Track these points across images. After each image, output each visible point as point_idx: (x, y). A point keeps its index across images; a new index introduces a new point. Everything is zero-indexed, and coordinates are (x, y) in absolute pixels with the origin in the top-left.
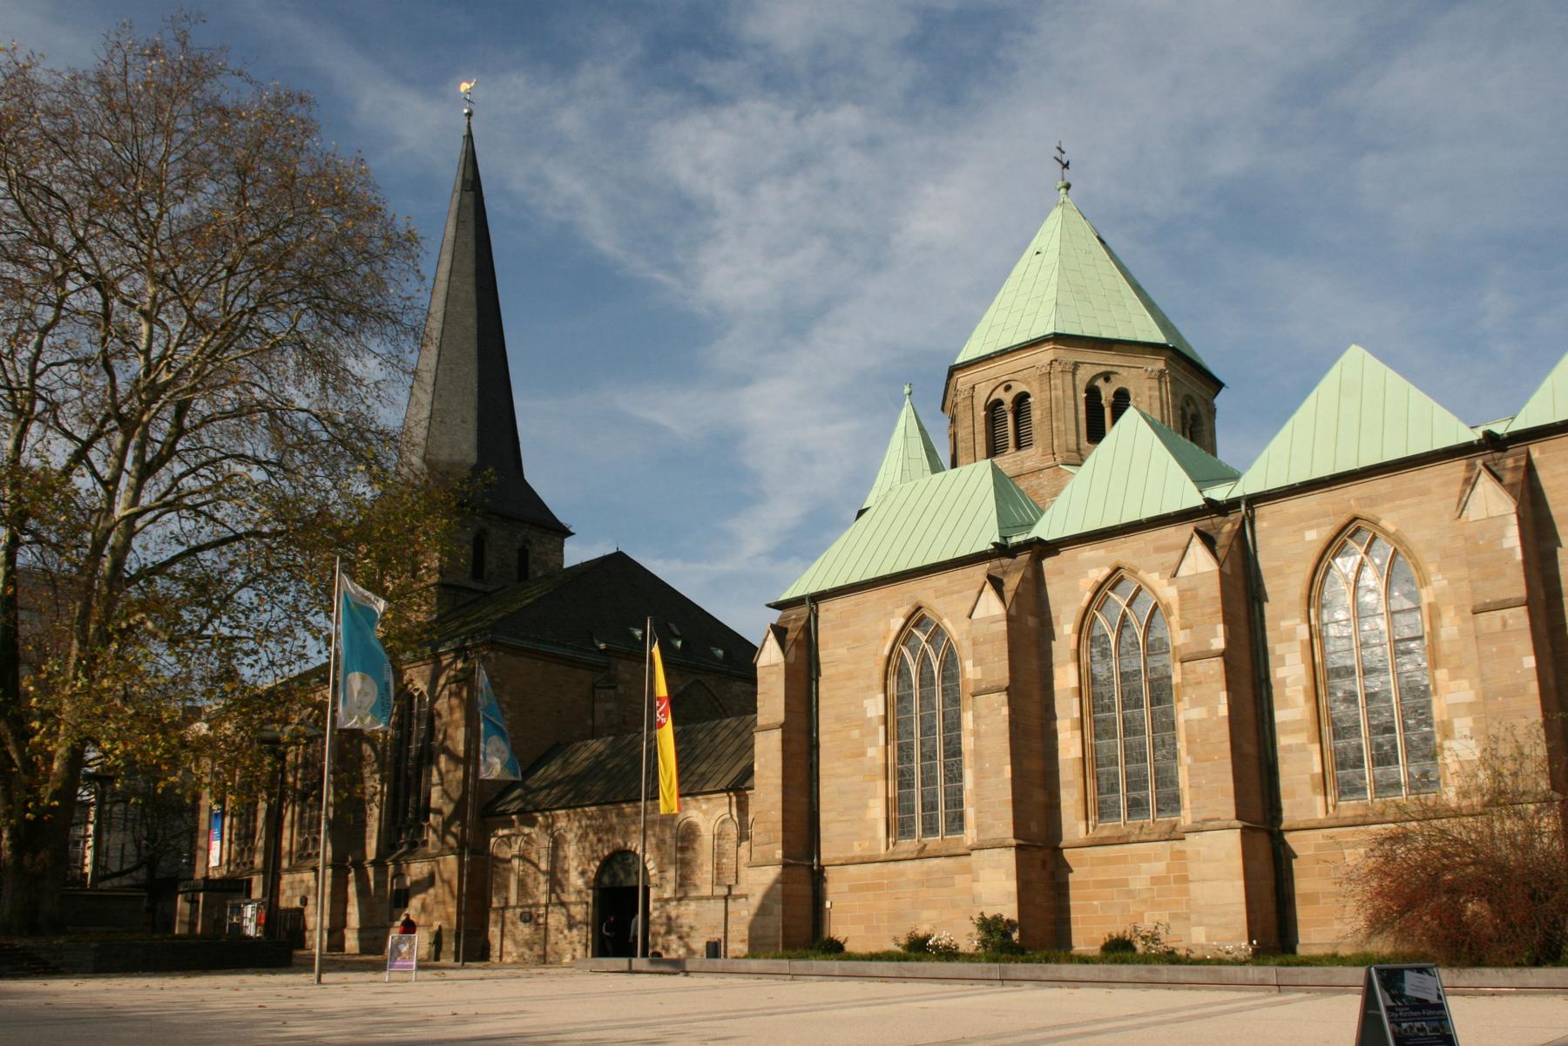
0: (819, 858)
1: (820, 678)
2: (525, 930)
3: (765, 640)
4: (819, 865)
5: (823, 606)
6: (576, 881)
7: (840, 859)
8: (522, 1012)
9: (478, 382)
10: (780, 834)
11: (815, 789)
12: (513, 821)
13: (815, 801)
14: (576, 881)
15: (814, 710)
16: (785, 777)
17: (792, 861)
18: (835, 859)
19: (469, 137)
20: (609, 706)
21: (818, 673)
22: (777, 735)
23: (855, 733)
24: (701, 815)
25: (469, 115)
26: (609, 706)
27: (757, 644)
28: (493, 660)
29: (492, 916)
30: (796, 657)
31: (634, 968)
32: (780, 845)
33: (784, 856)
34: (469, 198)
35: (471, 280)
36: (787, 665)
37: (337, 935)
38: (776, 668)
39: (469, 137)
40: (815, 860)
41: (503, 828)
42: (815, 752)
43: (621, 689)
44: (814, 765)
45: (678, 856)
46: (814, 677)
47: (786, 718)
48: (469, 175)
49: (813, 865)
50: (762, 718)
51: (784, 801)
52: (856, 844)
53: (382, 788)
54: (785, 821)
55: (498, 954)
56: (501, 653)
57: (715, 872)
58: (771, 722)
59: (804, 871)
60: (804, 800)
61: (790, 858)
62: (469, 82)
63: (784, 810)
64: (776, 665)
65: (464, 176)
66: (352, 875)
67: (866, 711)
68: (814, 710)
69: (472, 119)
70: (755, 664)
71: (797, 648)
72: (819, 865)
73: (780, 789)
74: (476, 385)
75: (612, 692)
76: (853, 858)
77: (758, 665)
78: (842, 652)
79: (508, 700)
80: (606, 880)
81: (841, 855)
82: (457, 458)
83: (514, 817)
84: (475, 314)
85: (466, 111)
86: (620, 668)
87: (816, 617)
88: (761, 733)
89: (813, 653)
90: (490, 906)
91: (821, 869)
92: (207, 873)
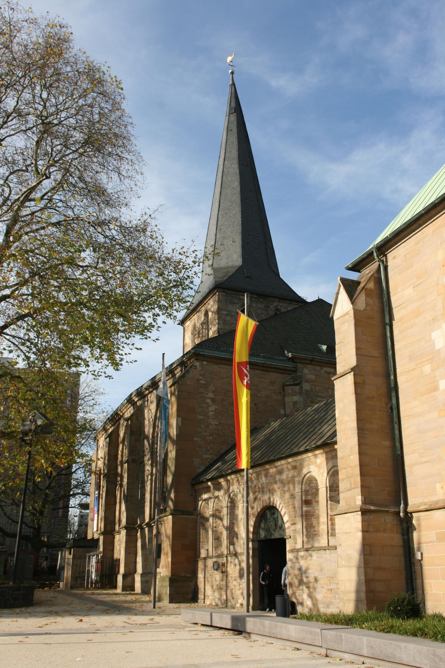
0: (406, 504)
1: (394, 322)
2: (218, 576)
3: (338, 294)
4: (406, 512)
5: (391, 255)
6: (242, 533)
7: (425, 504)
8: (257, 640)
9: (242, 217)
10: (358, 479)
11: (397, 432)
12: (209, 487)
13: (398, 444)
14: (242, 533)
15: (390, 353)
16: (359, 420)
17: (372, 508)
18: (421, 504)
19: (233, 84)
20: (295, 398)
21: (391, 318)
22: (350, 378)
23: (427, 369)
24: (316, 469)
25: (232, 73)
26: (295, 398)
27: (332, 302)
28: (198, 367)
29: (200, 565)
30: (367, 304)
31: (214, 625)
32: (359, 490)
33: (364, 502)
34: (234, 118)
35: (236, 161)
36: (356, 312)
37: (129, 579)
38: (347, 317)
39: (233, 84)
40: (402, 506)
41: (205, 493)
42: (394, 394)
43: (306, 386)
44: (395, 406)
45: (305, 509)
46: (387, 321)
47: (358, 361)
48: (233, 105)
49: (399, 512)
50: (340, 369)
51: (360, 444)
52: (438, 486)
53: (152, 470)
54: (362, 465)
55: (203, 597)
56: (205, 363)
57: (329, 523)
58: (346, 368)
59: (389, 519)
60: (387, 443)
61: (369, 504)
62: (231, 56)
63: (361, 454)
64: (347, 314)
65: (230, 106)
66: (139, 534)
67: (434, 344)
68: (390, 353)
69: (234, 75)
70: (332, 318)
71: (367, 296)
72: (406, 512)
73: (356, 432)
74: (240, 220)
75: (297, 388)
76: (437, 502)
77: (335, 318)
78: (409, 291)
79: (213, 396)
80: (263, 534)
81: (426, 500)
82: (230, 264)
83: (209, 483)
84: (238, 180)
85: (230, 71)
86: (306, 371)
87: (386, 268)
88: (338, 380)
89: (385, 299)
90: (199, 557)
91: (408, 517)
92: (93, 535)
